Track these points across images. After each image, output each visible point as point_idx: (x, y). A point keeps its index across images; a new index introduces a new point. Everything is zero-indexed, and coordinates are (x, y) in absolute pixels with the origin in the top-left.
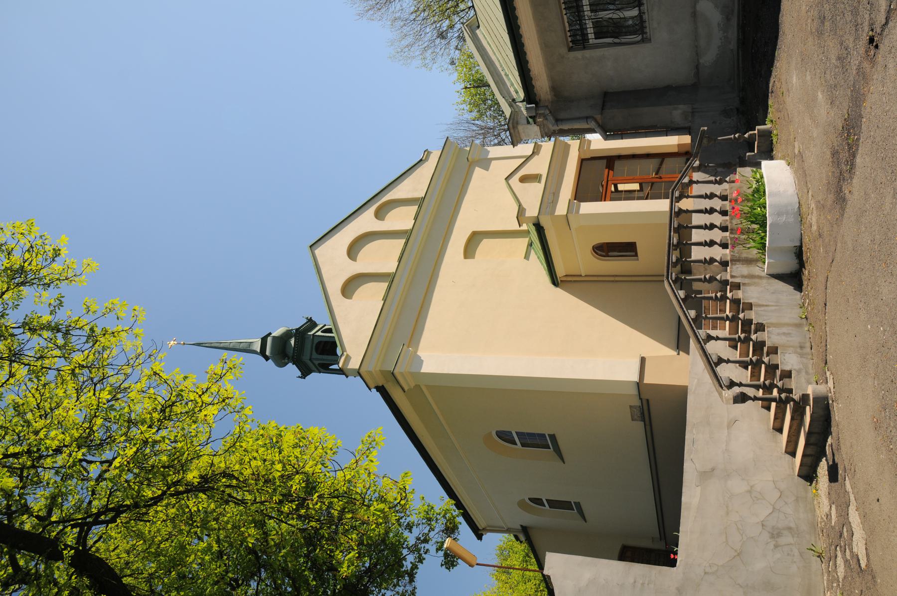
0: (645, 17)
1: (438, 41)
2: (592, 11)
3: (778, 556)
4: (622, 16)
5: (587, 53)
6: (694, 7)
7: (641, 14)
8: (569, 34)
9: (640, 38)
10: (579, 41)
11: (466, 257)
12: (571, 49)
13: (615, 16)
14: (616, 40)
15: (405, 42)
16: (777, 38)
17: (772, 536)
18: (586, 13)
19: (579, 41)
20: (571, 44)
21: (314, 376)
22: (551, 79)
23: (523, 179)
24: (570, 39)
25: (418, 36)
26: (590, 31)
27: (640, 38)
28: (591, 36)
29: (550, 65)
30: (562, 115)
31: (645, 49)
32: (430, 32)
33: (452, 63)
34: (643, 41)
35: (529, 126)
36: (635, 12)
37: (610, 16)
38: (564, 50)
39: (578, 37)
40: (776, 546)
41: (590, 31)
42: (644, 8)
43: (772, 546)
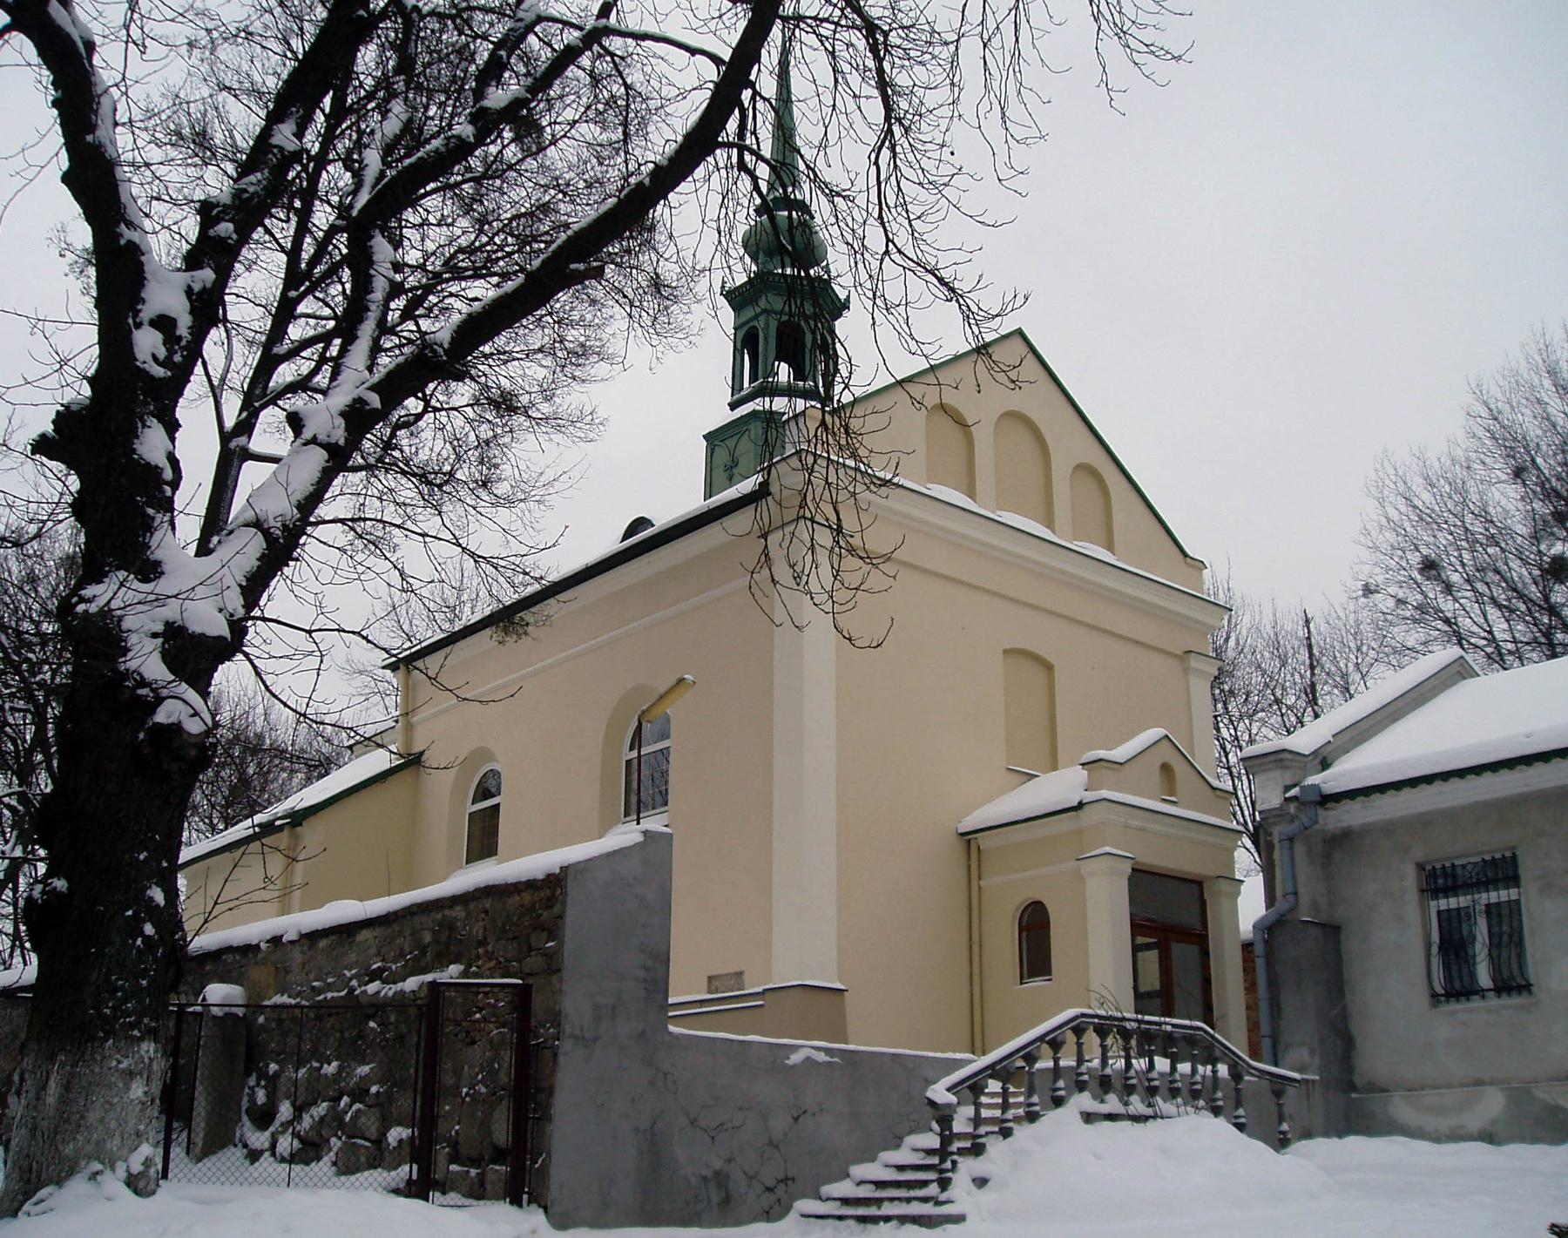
0: (1476, 1003)
1: (1415, 559)
2: (1488, 906)
3: (693, 1180)
4: (1478, 959)
5: (1412, 896)
6: (1492, 1083)
7: (1481, 993)
8: (1448, 864)
9: (1440, 991)
10: (1439, 880)
11: (1005, 651)
12: (1420, 867)
13: (1478, 947)
14: (1435, 949)
15: (1417, 484)
16: (494, 886)
17: (717, 1173)
18: (1484, 895)
19: (1439, 880)
20: (1429, 867)
21: (727, 315)
22: (1366, 830)
23: (1166, 768)
24: (1438, 866)
25: (1426, 519)
26: (1453, 902)
27: (1440, 991)
28: (1443, 904)
29: (1389, 829)
30: (1300, 849)
31: (1421, 998)
32: (1436, 543)
33: (1368, 591)
34: (1434, 996)
35: (1280, 789)
36: (1484, 978)
37: (1479, 938)
38: (1419, 854)
39: (1440, 881)
40: (705, 1179)
41: (1453, 902)
42: (1494, 1001)
43: (705, 1172)
